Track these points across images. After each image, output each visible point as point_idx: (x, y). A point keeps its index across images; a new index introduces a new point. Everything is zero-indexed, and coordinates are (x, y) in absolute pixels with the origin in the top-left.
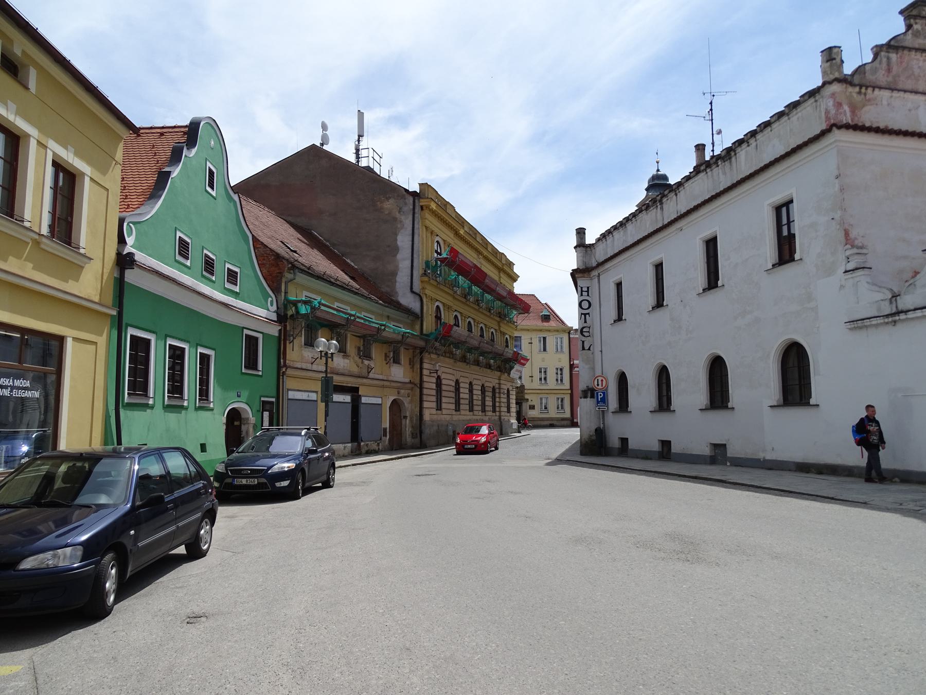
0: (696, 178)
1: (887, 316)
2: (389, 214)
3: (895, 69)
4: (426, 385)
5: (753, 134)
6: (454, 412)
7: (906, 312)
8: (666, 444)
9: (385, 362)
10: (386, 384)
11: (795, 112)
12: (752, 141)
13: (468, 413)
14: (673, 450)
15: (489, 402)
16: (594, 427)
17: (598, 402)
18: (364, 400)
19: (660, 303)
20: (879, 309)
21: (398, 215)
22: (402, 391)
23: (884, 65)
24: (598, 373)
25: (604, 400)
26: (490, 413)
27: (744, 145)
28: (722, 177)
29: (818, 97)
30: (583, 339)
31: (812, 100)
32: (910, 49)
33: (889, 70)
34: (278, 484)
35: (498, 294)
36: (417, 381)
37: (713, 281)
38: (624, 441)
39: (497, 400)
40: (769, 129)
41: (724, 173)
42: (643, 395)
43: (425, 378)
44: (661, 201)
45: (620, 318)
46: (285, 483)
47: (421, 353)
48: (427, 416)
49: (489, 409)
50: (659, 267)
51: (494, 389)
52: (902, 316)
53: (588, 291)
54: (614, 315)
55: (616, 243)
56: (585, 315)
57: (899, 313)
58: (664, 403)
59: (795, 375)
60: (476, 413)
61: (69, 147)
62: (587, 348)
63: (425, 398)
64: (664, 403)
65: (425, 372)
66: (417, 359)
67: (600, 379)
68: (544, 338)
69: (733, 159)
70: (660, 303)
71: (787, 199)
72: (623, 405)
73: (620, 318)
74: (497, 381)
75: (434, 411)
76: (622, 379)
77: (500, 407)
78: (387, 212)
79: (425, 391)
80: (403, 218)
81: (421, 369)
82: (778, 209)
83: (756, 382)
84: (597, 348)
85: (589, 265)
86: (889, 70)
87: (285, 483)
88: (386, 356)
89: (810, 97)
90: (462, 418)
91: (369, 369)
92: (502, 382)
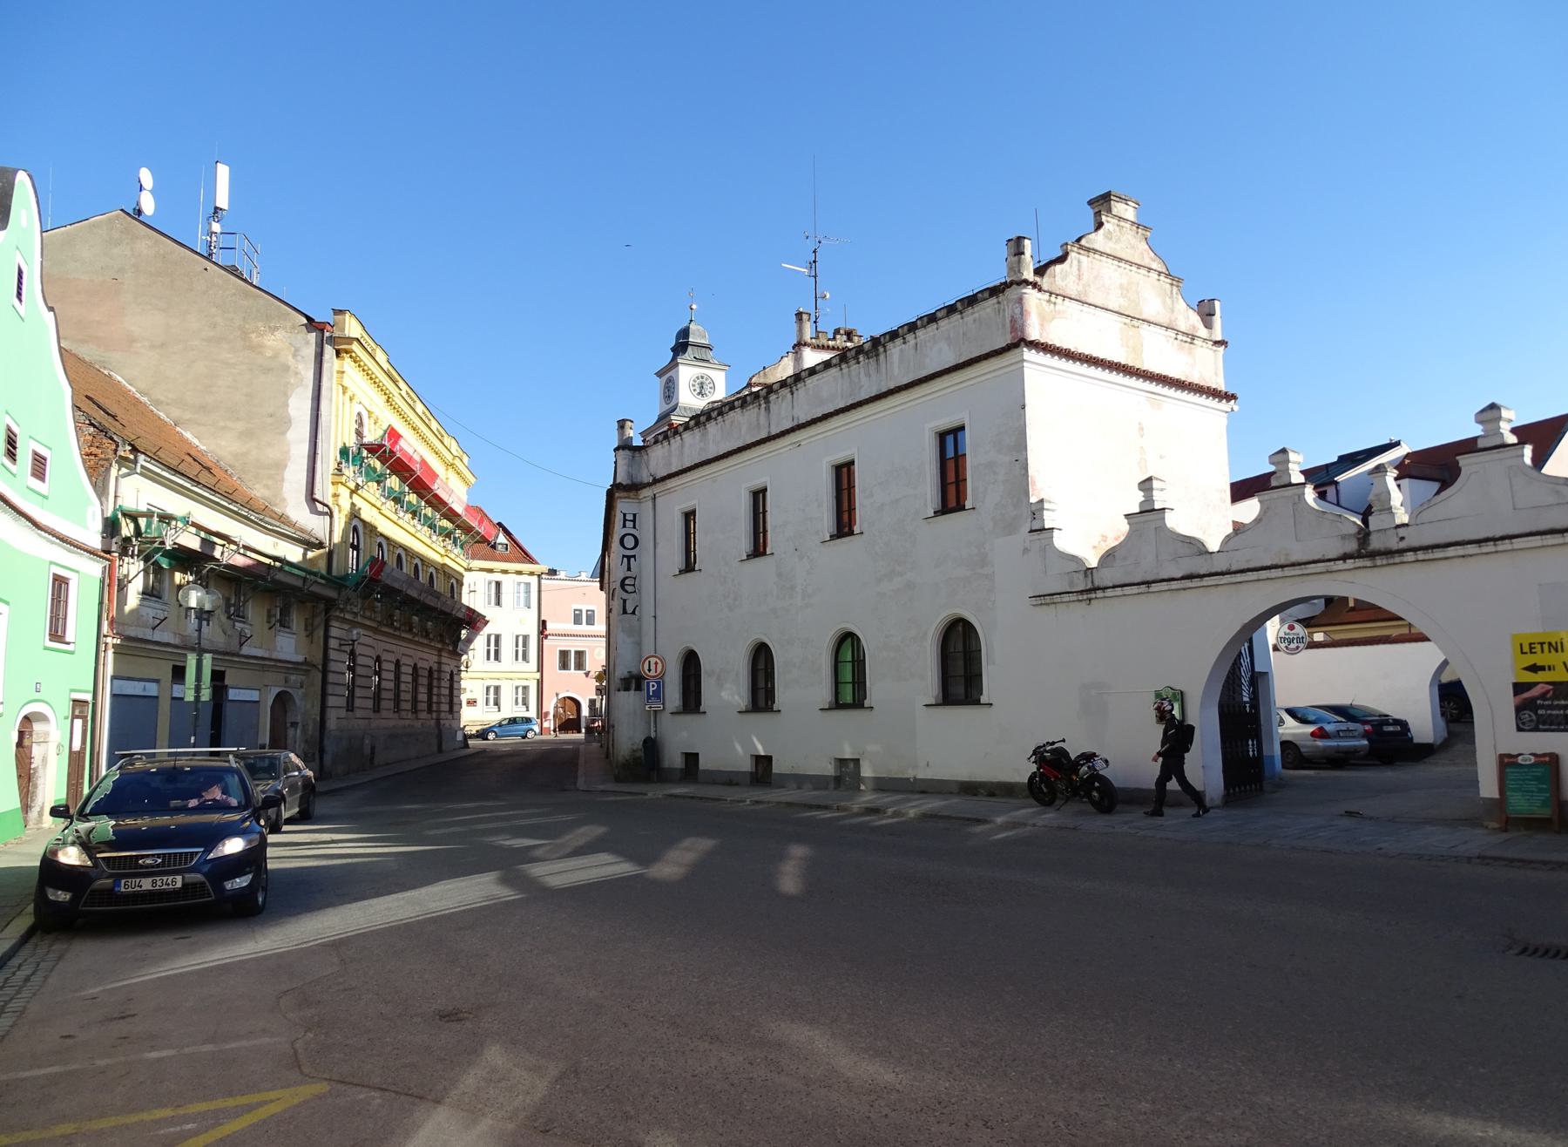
0: (825, 374)
1: (1082, 592)
2: (276, 356)
3: (1085, 278)
4: (333, 666)
5: (912, 327)
6: (371, 714)
7: (1104, 589)
8: (763, 762)
9: (267, 626)
10: (267, 665)
11: (970, 310)
12: (910, 337)
13: (391, 715)
14: (775, 770)
15: (423, 697)
16: (639, 738)
17: (649, 697)
18: (233, 694)
19: (759, 549)
20: (1071, 584)
21: (291, 361)
22: (293, 678)
23: (1075, 269)
24: (648, 649)
25: (658, 694)
26: (423, 715)
27: (899, 341)
28: (864, 378)
29: (1001, 297)
30: (625, 596)
31: (993, 300)
32: (1102, 254)
33: (1079, 277)
34: (228, 885)
35: (451, 510)
36: (318, 659)
37: (844, 526)
38: (692, 758)
39: (435, 691)
40: (934, 326)
41: (868, 375)
42: (726, 689)
43: (333, 655)
44: (766, 398)
45: (689, 567)
46: (242, 882)
47: (327, 611)
48: (332, 723)
49: (406, 706)
50: (759, 496)
51: (431, 671)
52: (1100, 594)
53: (634, 521)
54: (678, 561)
55: (686, 450)
56: (629, 558)
57: (1095, 589)
58: (762, 696)
59: (960, 665)
60: (403, 714)
61: (1033, 500)
62: (630, 610)
63: (330, 689)
64: (762, 696)
65: (333, 643)
66: (319, 620)
67: (653, 660)
68: (498, 584)
69: (882, 357)
70: (759, 549)
71: (956, 424)
72: (692, 700)
73: (689, 567)
74: (435, 658)
75: (343, 713)
76: (691, 661)
77: (439, 703)
78: (269, 354)
79: (331, 678)
80: (301, 367)
81: (327, 637)
82: (942, 436)
83: (905, 671)
84: (647, 610)
85: (638, 480)
86: (1079, 277)
87: (242, 882)
88: (270, 616)
89: (991, 296)
90: (384, 723)
91: (243, 639)
92: (444, 660)
